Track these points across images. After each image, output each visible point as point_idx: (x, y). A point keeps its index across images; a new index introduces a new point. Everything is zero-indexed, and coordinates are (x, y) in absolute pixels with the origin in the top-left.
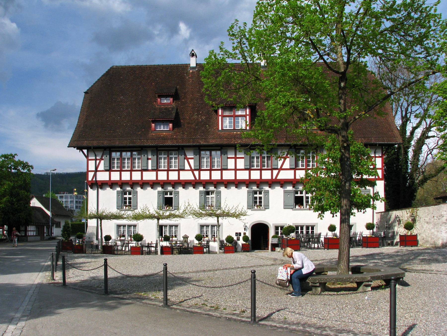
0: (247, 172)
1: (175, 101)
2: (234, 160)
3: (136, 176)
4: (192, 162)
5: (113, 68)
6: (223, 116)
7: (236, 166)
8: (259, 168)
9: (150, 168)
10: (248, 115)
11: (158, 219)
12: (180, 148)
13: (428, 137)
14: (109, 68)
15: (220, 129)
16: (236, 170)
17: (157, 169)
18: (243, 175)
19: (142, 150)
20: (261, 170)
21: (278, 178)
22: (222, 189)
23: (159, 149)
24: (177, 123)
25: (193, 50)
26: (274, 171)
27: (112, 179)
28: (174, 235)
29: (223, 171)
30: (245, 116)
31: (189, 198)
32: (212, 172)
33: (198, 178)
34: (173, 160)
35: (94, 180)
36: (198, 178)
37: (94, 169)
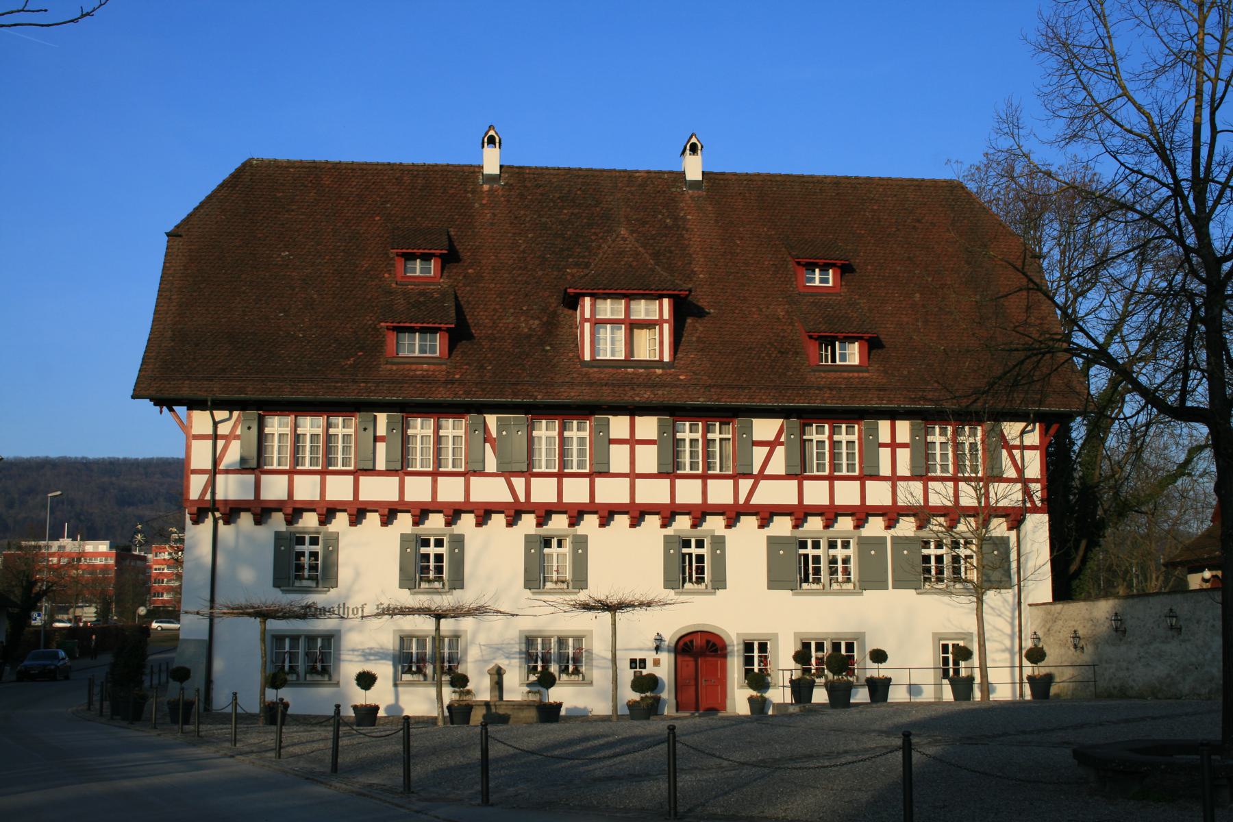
5: (251, 166)
6: (597, 323)
9: (381, 465)
10: (666, 321)
13: (171, 410)
14: (238, 165)
15: (587, 357)
17: (401, 468)
18: (654, 492)
21: (753, 501)
25: (491, 127)
27: (328, 498)
29: (362, 479)
30: (659, 323)
31: (495, 553)
32: (709, 481)
33: (522, 499)
35: (208, 497)
36: (522, 499)
37: (209, 466)
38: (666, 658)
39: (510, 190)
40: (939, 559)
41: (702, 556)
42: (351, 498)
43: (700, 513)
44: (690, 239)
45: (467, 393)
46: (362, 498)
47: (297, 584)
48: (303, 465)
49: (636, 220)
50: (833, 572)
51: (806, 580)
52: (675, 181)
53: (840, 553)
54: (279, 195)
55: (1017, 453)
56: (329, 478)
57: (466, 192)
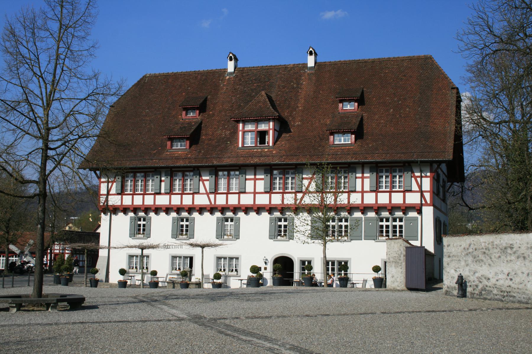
0: (374, 194)
1: (201, 114)
2: (253, 181)
3: (149, 200)
4: (207, 184)
7: (255, 188)
8: (389, 190)
9: (163, 191)
11: (142, 249)
12: (407, 164)
14: (141, 77)
15: (240, 146)
16: (363, 192)
18: (263, 200)
19: (156, 171)
20: (390, 192)
22: (241, 215)
23: (379, 165)
24: (359, 134)
26: (298, 194)
27: (134, 204)
28: (145, 266)
33: (213, 203)
34: (384, 179)
36: (213, 203)
37: (106, 193)
38: (270, 267)
39: (236, 78)
40: (387, 227)
41: (388, 226)
42: (388, 202)
43: (283, 209)
44: (301, 93)
45: (189, 162)
46: (134, 204)
47: (137, 236)
48: (233, 190)
49: (282, 86)
50: (395, 232)
51: (182, 235)
52: (304, 67)
53: (398, 223)
54: (152, 87)
55: (419, 179)
56: (184, 196)
57: (220, 80)
